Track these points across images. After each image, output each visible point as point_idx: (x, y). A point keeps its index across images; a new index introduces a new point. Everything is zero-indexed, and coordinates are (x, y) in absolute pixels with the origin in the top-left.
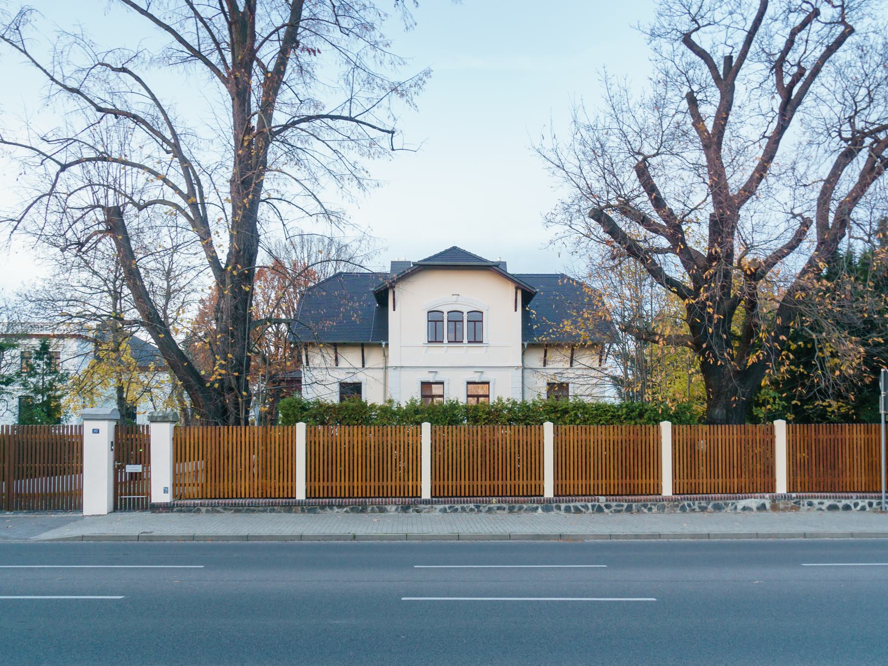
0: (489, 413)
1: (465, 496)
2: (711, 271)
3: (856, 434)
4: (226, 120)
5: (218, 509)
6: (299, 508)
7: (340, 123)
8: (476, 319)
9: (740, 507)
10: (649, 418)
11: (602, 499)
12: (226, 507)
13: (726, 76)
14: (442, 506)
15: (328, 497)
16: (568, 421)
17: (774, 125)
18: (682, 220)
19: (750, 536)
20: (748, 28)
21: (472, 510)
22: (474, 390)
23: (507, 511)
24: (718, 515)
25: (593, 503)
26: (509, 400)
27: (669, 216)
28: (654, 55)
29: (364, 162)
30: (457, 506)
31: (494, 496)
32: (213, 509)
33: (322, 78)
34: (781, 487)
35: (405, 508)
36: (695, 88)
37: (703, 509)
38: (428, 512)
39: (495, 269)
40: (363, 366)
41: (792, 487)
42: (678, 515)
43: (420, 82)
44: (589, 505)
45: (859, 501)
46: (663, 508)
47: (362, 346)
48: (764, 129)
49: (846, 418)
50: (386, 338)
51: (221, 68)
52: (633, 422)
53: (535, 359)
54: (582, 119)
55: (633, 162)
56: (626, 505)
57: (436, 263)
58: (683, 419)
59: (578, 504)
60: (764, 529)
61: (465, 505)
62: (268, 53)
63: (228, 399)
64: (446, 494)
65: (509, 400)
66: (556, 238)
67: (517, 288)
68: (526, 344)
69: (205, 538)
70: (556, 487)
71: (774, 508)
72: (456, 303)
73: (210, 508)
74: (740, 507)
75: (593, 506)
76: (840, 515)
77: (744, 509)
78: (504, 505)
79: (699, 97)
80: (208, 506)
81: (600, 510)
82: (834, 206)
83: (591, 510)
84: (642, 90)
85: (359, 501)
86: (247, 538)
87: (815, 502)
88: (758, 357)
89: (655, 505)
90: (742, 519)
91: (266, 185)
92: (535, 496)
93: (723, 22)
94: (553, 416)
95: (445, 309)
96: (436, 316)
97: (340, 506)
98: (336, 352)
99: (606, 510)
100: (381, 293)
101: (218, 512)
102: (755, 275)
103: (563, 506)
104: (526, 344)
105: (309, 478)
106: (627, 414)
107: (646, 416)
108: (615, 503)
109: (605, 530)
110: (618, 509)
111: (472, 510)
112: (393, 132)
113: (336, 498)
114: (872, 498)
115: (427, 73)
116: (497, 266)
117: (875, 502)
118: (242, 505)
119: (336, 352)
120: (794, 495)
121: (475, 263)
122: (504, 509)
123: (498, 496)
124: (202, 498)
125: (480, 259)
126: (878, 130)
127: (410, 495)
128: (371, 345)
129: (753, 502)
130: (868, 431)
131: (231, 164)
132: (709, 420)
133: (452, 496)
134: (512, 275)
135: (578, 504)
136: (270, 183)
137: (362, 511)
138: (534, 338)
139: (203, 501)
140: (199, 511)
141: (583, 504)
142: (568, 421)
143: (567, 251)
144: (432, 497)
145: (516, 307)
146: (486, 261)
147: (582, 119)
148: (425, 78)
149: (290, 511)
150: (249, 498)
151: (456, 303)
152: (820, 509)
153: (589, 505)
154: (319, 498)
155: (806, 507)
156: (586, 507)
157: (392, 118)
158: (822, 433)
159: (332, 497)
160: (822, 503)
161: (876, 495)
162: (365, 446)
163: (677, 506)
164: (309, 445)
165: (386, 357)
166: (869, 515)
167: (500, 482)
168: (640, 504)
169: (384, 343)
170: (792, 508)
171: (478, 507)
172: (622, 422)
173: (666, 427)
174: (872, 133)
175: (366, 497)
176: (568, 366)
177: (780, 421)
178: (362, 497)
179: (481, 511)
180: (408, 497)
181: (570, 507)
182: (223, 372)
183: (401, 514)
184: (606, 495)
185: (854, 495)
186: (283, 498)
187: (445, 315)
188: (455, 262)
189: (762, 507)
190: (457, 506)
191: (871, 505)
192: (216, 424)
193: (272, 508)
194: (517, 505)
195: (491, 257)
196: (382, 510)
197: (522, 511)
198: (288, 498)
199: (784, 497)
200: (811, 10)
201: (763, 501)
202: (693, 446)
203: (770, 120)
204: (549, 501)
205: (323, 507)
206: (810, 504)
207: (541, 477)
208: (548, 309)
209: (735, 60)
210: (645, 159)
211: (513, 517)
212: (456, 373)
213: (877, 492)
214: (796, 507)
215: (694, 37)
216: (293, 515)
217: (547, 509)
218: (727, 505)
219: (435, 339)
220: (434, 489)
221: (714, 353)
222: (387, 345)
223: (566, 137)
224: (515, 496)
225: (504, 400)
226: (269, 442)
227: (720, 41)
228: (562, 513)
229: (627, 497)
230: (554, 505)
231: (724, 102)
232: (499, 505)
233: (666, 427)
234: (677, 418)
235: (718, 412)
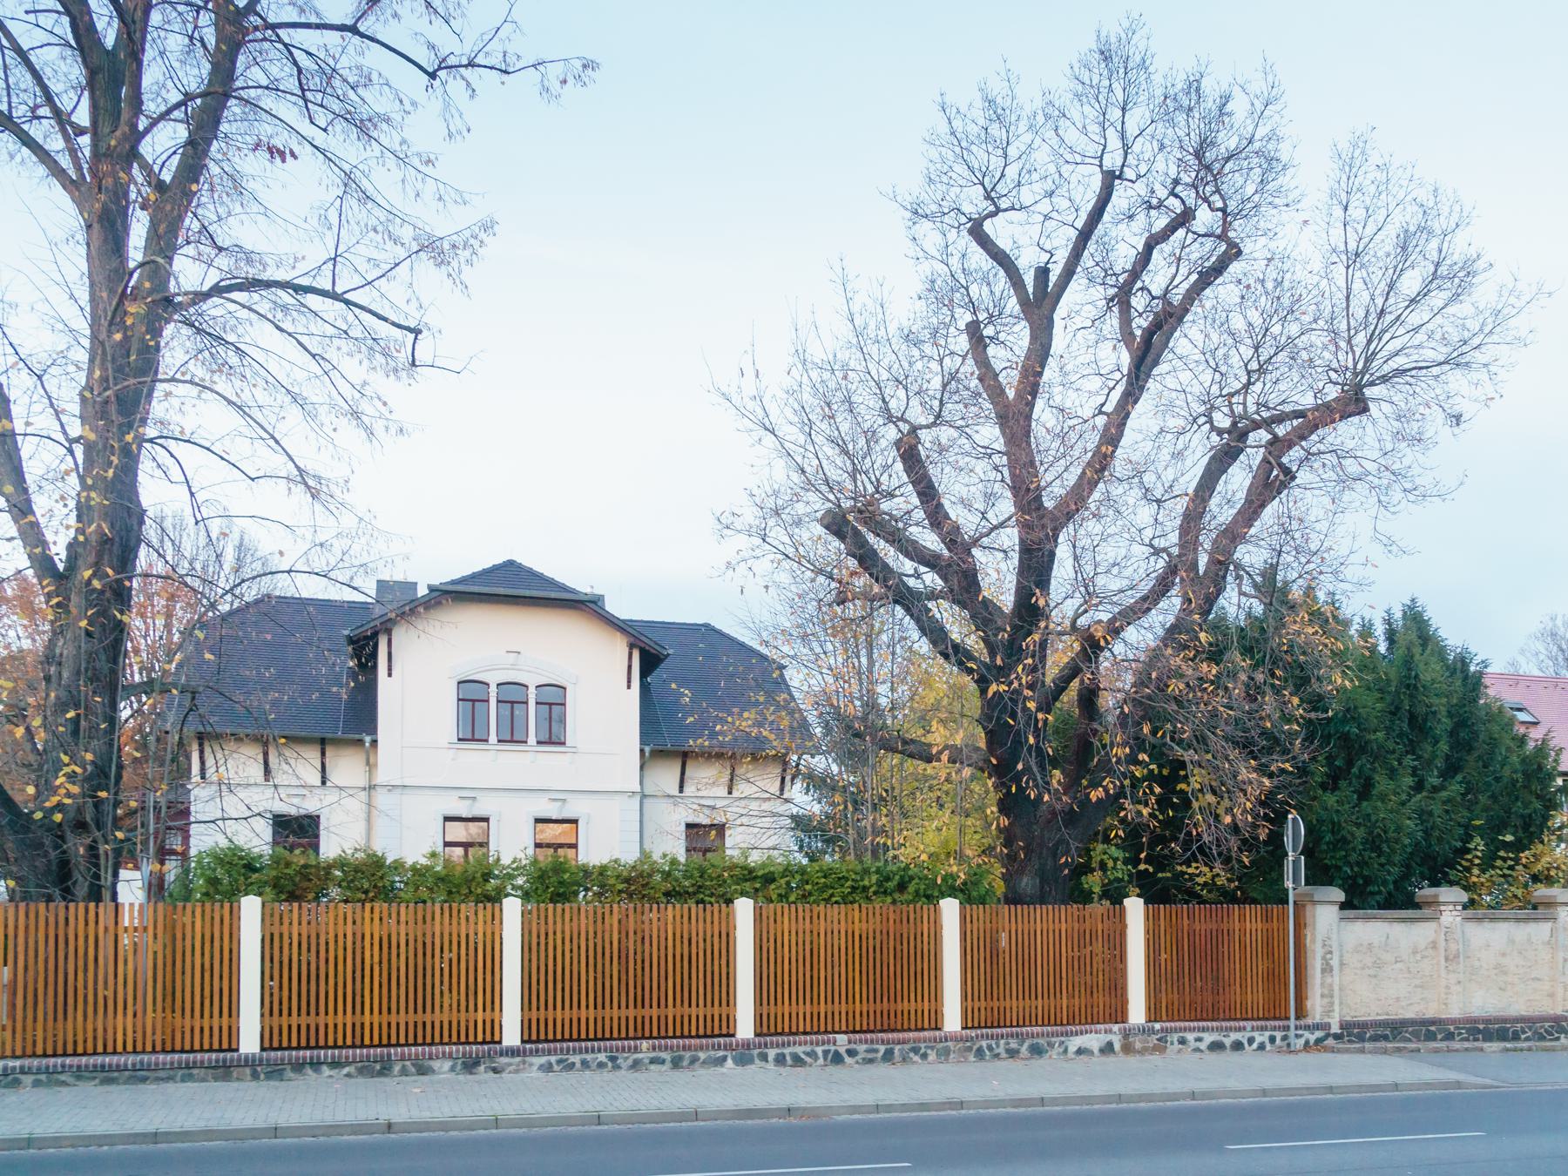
0: (627, 881)
1: (588, 1039)
2: (1036, 637)
3: (1248, 921)
4: (76, 262)
5: (63, 1077)
6: (248, 1071)
7: (312, 300)
8: (554, 703)
9: (1072, 1049)
10: (917, 892)
11: (842, 1039)
12: (80, 1074)
13: (1040, 303)
14: (543, 1060)
15: (308, 1047)
16: (774, 897)
17: (1116, 396)
18: (976, 542)
19: (1107, 1099)
20: (1079, 224)
21: (601, 1065)
22: (458, 832)
23: (668, 1065)
24: (1038, 1063)
25: (826, 1047)
26: (665, 856)
27: (952, 537)
28: (913, 251)
29: (381, 383)
30: (572, 1059)
31: (643, 1038)
32: (50, 1079)
33: (272, 205)
34: (1137, 1013)
35: (470, 1065)
36: (982, 316)
37: (1013, 1054)
38: (517, 1071)
39: (587, 606)
40: (324, 783)
41: (1154, 1013)
42: (973, 1067)
43: (472, 241)
44: (819, 1050)
45: (1256, 1034)
46: (946, 1052)
47: (323, 743)
48: (1101, 399)
49: (1228, 897)
50: (373, 730)
51: (65, 162)
52: (889, 900)
53: (665, 777)
54: (817, 354)
55: (891, 433)
56: (882, 1048)
57: (476, 589)
58: (975, 894)
59: (799, 1050)
60: (1127, 1087)
61: (589, 1057)
62: (163, 144)
63: (78, 847)
64: (551, 1037)
65: (665, 856)
66: (739, 558)
67: (631, 646)
68: (647, 749)
69: (57, 1141)
70: (759, 1019)
71: (1127, 1049)
72: (513, 667)
73: (43, 1077)
74: (1072, 1049)
75: (826, 1053)
76: (1229, 1057)
77: (1080, 1051)
78: (664, 1055)
79: (988, 331)
80: (39, 1071)
81: (837, 1059)
82: (1206, 541)
83: (821, 1061)
84: (906, 307)
85: (378, 1049)
86: (155, 1137)
87: (1190, 1037)
88: (1106, 790)
89: (932, 1048)
90: (1076, 1071)
91: (158, 408)
92: (720, 1035)
93: (1038, 207)
94: (747, 886)
95: (493, 679)
96: (473, 692)
97: (335, 1064)
98: (323, 754)
99: (848, 1060)
100: (364, 639)
101: (64, 1084)
102: (1092, 647)
103: (772, 1053)
104: (647, 749)
105: (269, 1006)
106: (880, 884)
107: (911, 889)
108: (864, 1047)
109: (867, 1096)
110: (870, 1056)
111: (601, 1065)
112: (416, 332)
113: (326, 1047)
114: (1274, 1029)
115: (488, 226)
116: (594, 602)
117: (1279, 1035)
118: (118, 1069)
119: (323, 754)
120: (1157, 1026)
121: (553, 595)
122: (663, 1062)
123: (651, 1037)
124: (24, 1056)
125: (551, 583)
126: (1280, 419)
127: (480, 1039)
128: (338, 742)
129: (1093, 1040)
130: (1267, 918)
131: (82, 356)
132: (1013, 899)
133: (563, 1040)
134: (624, 621)
135: (799, 1050)
136: (169, 406)
137: (381, 1073)
138: (666, 740)
139: (27, 1062)
140: (16, 1083)
141: (808, 1048)
142: (774, 897)
143: (742, 584)
144: (523, 1041)
145: (629, 681)
146: (573, 591)
147: (817, 354)
148: (482, 235)
149: (226, 1077)
150: (135, 1052)
151: (513, 667)
152: (1198, 1050)
153: (819, 1050)
154: (289, 1048)
155: (1177, 1046)
156: (813, 1054)
157: (414, 304)
158: (1195, 920)
159: (317, 1047)
160: (1199, 1040)
161: (1281, 1023)
162: (385, 944)
163: (970, 1049)
164: (269, 942)
165: (371, 765)
166: (1268, 1060)
167: (670, 1012)
168: (907, 1047)
169: (368, 739)
170: (1155, 1049)
171: (613, 1059)
172: (868, 898)
173: (950, 908)
174: (1267, 424)
175: (389, 1045)
176: (723, 792)
177: (251, 897)
178: (380, 1045)
179: (619, 1067)
180: (476, 1043)
181: (784, 1056)
182: (75, 789)
183: (461, 1077)
184: (845, 1032)
185: (1248, 1024)
186: (211, 1050)
187: (493, 690)
188: (510, 589)
189: (1108, 1049)
190: (572, 1059)
191: (1272, 1040)
192: (49, 899)
193: (187, 1072)
194: (688, 1055)
195: (580, 582)
196: (423, 1071)
197: (697, 1065)
198: (221, 1050)
199: (1143, 1031)
200: (1179, 209)
201: (1109, 1037)
202: (995, 941)
203: (1111, 384)
204: (747, 1045)
205: (298, 1067)
206: (1182, 1041)
207: (729, 999)
208: (689, 688)
209: (1053, 278)
210: (914, 429)
211: (681, 1076)
212: (509, 800)
213: (1280, 1019)
214: (1161, 1047)
215: (988, 226)
216: (235, 1084)
217: (743, 1061)
218: (1051, 1045)
219: (471, 734)
220: (526, 1025)
221: (1035, 780)
222: (374, 742)
223: (777, 379)
224: (682, 1037)
225: (656, 857)
226: (179, 936)
227: (1032, 239)
228: (771, 1066)
229: (883, 1035)
230: (756, 1052)
231: (1038, 346)
232: (653, 1055)
233: (950, 908)
234: (968, 893)
235: (1027, 883)
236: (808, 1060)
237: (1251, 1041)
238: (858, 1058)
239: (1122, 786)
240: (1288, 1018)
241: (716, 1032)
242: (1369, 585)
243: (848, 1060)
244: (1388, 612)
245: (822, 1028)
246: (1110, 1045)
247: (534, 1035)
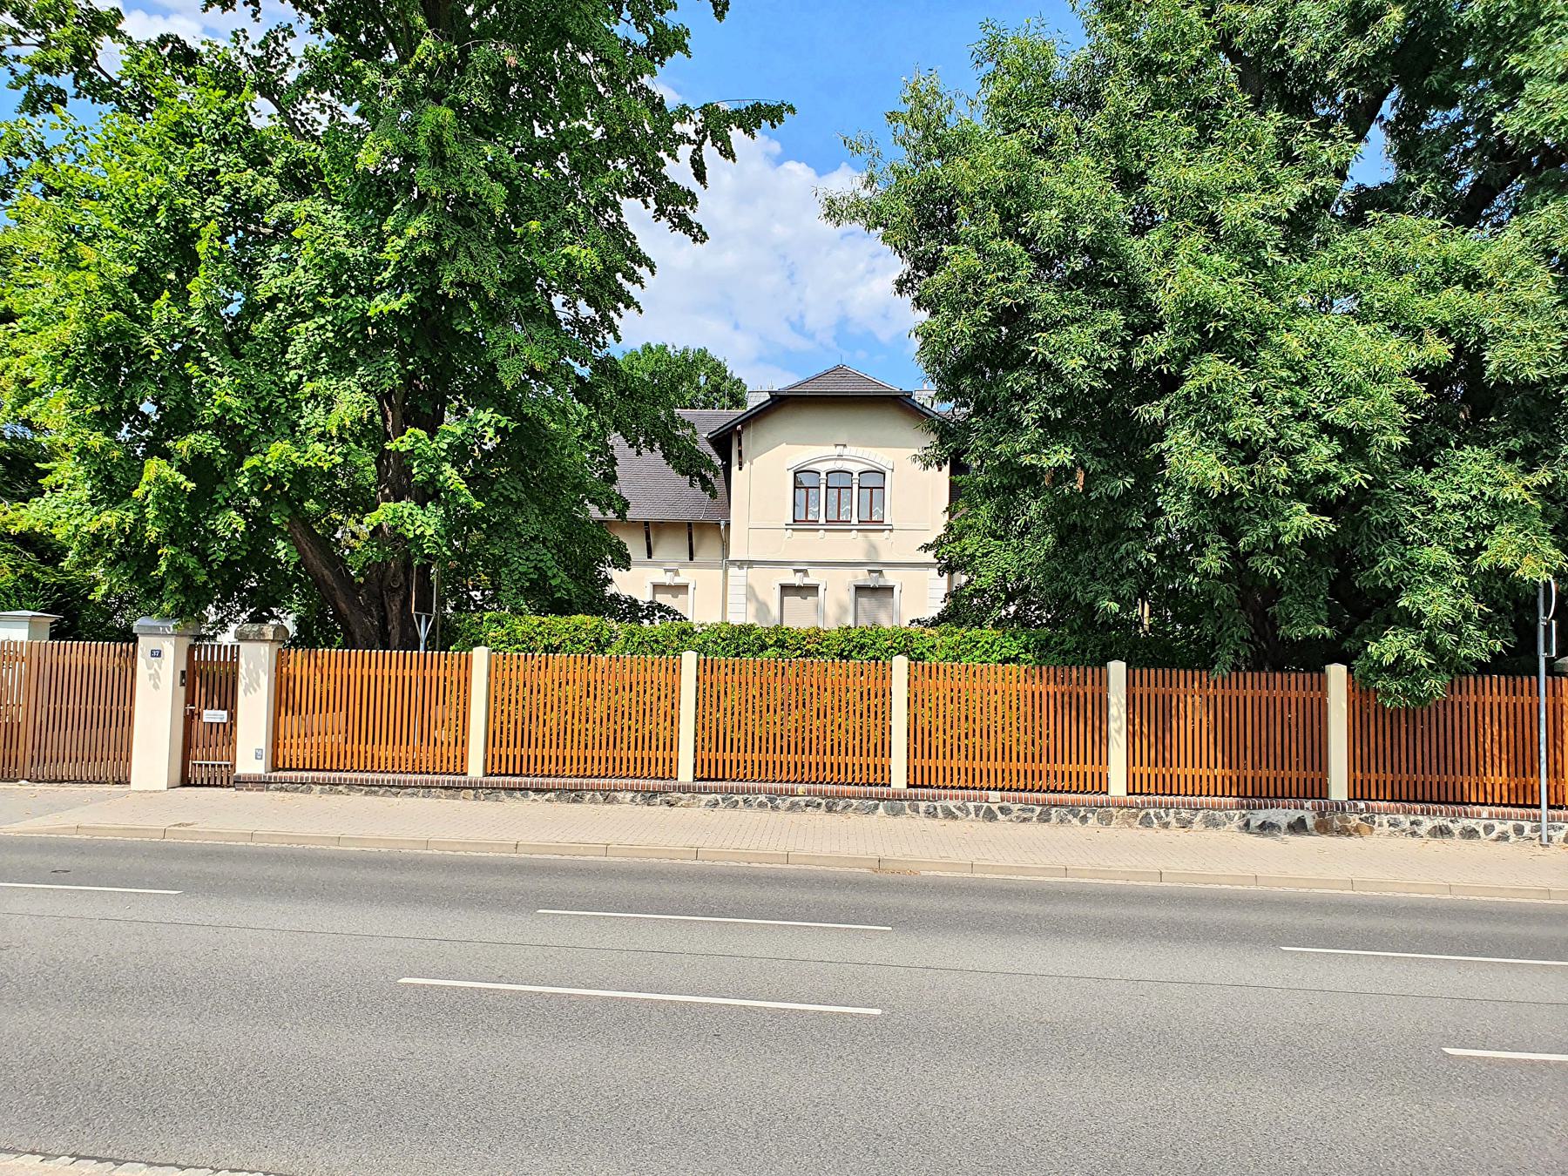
21: (761, 805)
38: (687, 806)
44: (971, 805)
45: (1495, 823)
56: (1038, 809)
59: (951, 804)
71: (1323, 828)
75: (977, 809)
76: (1456, 844)
81: (990, 816)
83: (973, 815)
111: (761, 805)
117: (1528, 826)
135: (951, 804)
153: (971, 805)
155: (1386, 828)
191: (1519, 830)
236: (958, 813)
237: (1489, 829)
238: (1013, 816)
239: (490, 620)
240: (1539, 807)
241: (1474, 800)
242: (684, 224)
243: (1000, 816)
244: (833, 211)
245: (973, 782)
246: (1301, 821)
247: (707, 773)
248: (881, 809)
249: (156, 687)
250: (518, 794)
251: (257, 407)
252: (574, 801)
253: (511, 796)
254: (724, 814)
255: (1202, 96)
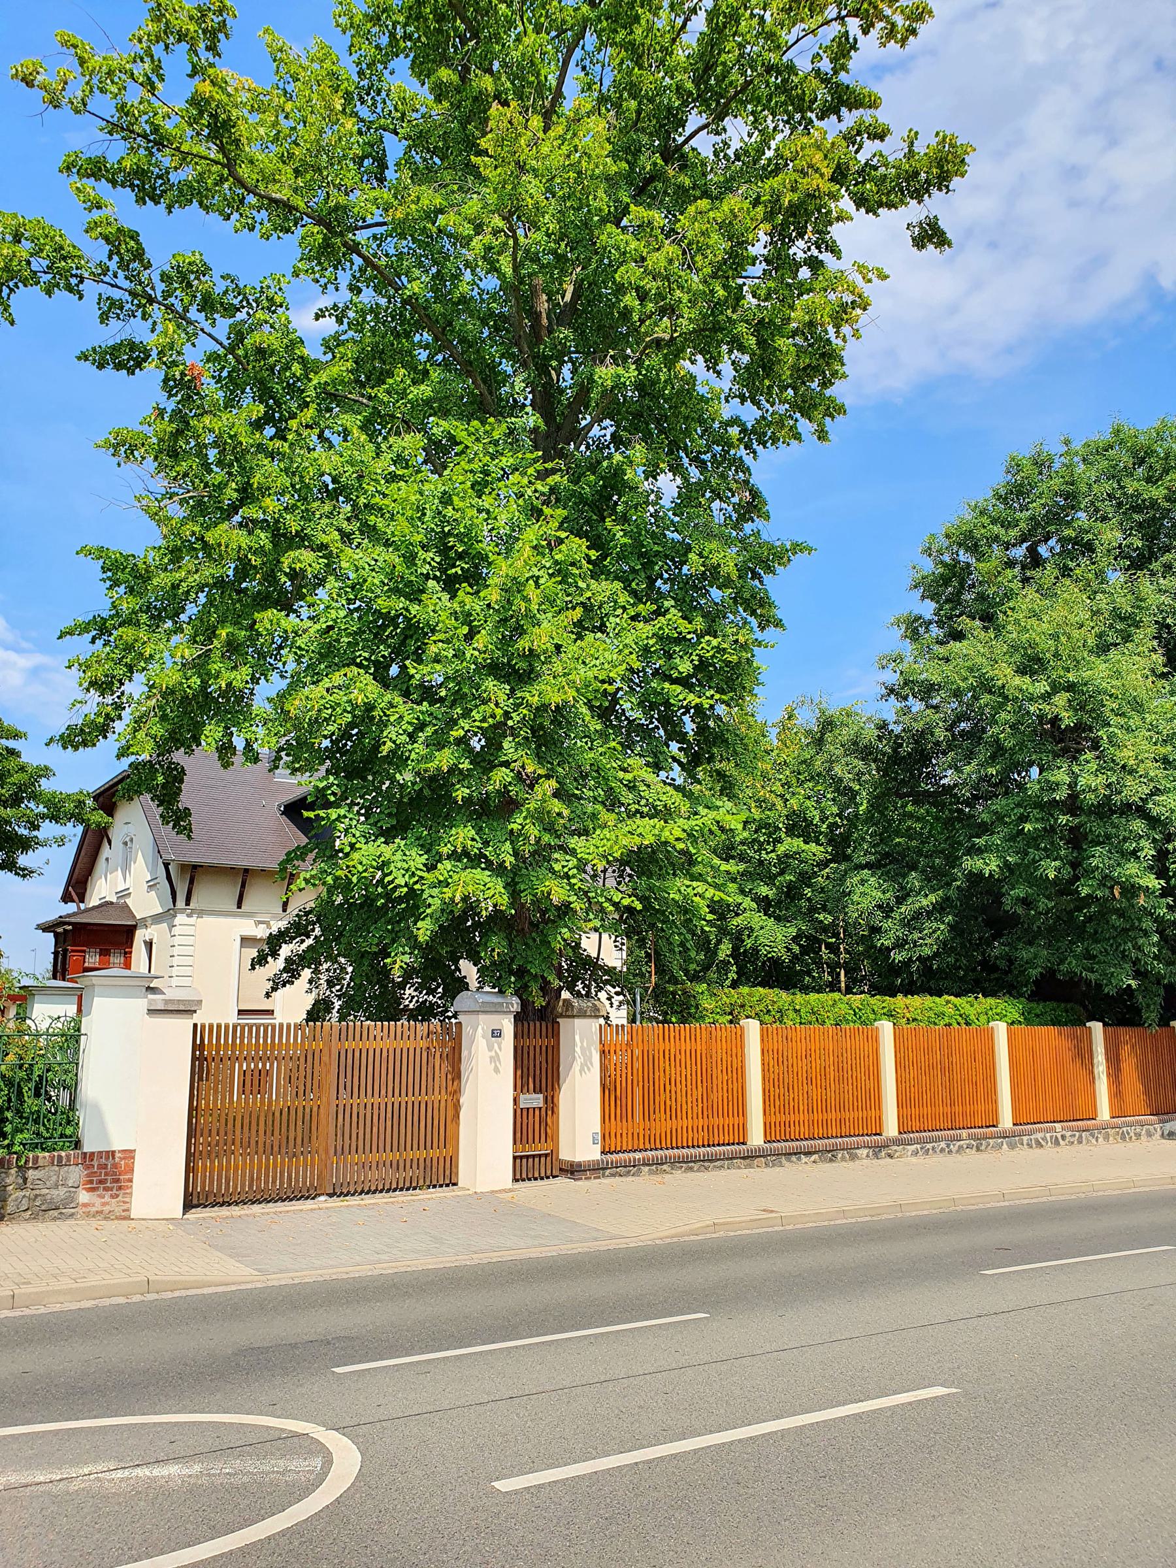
21: (942, 1150)
111: (942, 1150)
135: (1039, 1136)
248: (1005, 1146)
249: (497, 1070)
250: (794, 1158)
251: (865, 180)
252: (831, 1160)
253: (789, 1161)
254: (936, 1161)
255: (107, 1199)
